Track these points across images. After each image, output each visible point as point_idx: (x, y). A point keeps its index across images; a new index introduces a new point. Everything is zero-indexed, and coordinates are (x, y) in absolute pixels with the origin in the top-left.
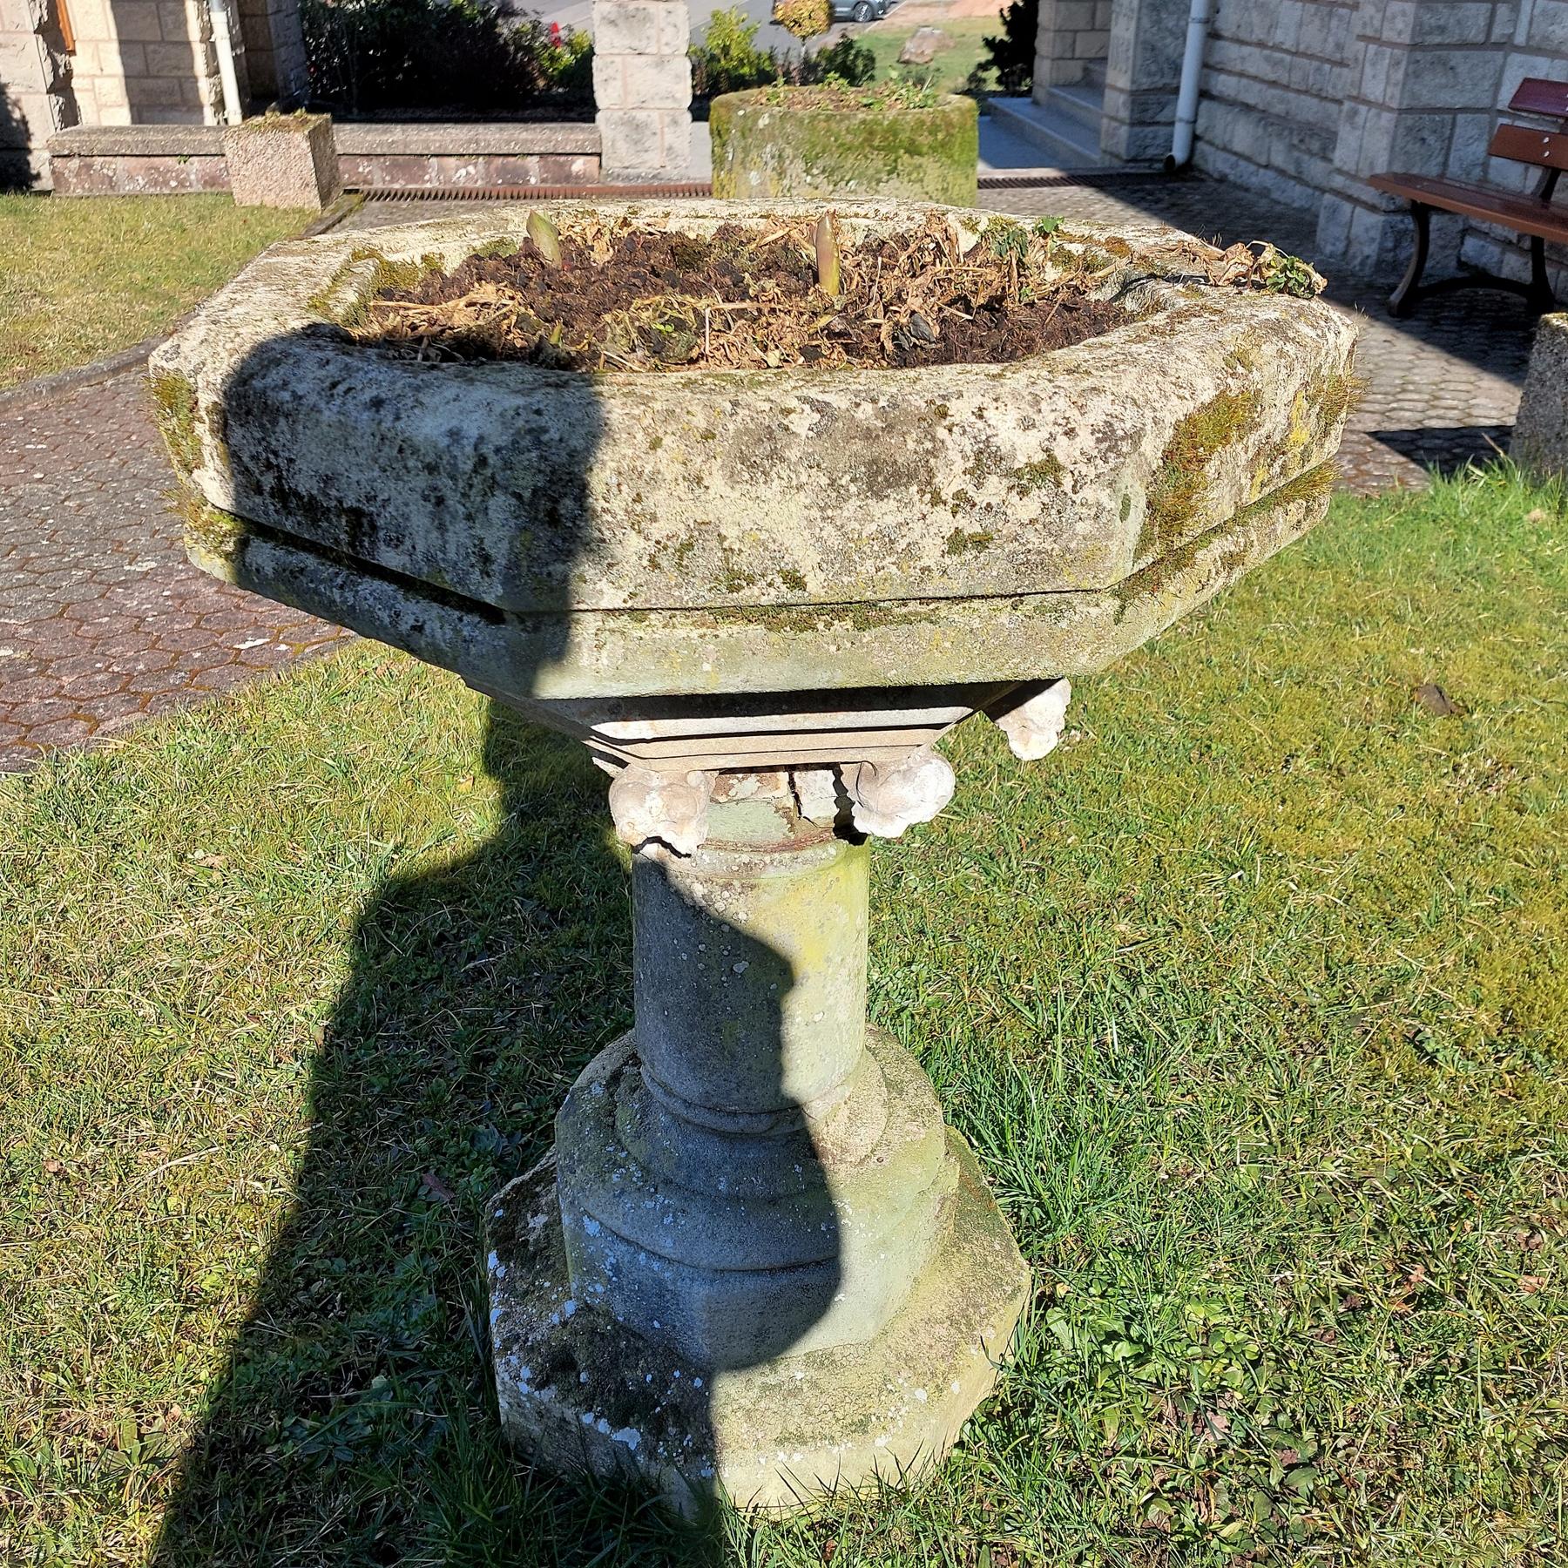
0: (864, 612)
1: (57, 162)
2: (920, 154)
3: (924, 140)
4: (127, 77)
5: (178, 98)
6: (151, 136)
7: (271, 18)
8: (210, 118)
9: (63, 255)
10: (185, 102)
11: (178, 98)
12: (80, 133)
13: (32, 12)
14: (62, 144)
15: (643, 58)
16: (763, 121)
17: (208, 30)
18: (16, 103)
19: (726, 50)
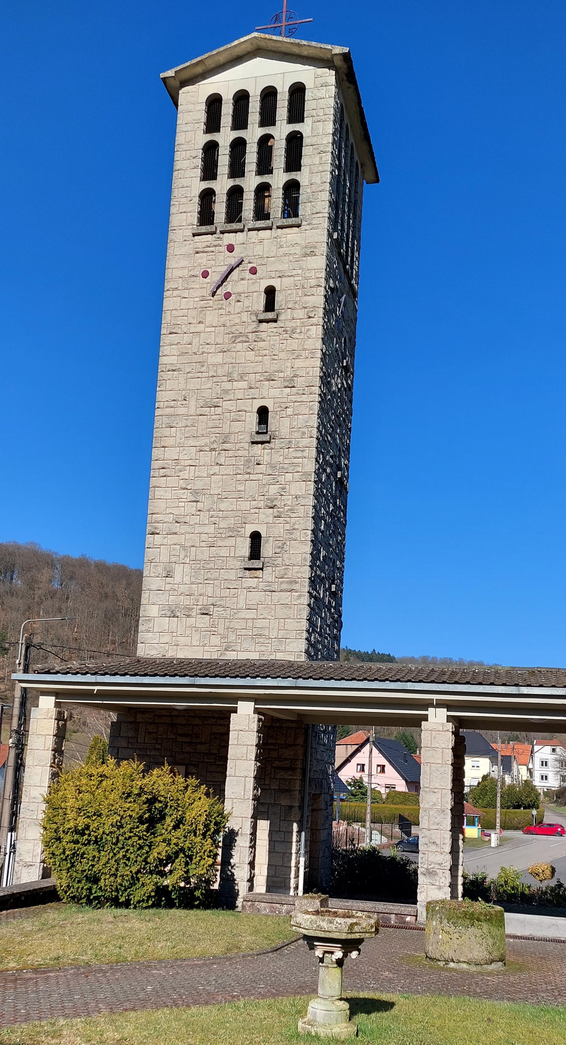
0: (329, 932)
1: (245, 903)
2: (481, 922)
3: (482, 918)
4: (268, 876)
5: (283, 885)
6: (274, 897)
7: (320, 859)
8: (292, 893)
9: (247, 927)
10: (285, 886)
11: (283, 885)
12: (253, 894)
13: (249, 858)
14: (247, 897)
15: (434, 886)
16: (437, 908)
17: (298, 863)
18: (237, 884)
19: (506, 882)
